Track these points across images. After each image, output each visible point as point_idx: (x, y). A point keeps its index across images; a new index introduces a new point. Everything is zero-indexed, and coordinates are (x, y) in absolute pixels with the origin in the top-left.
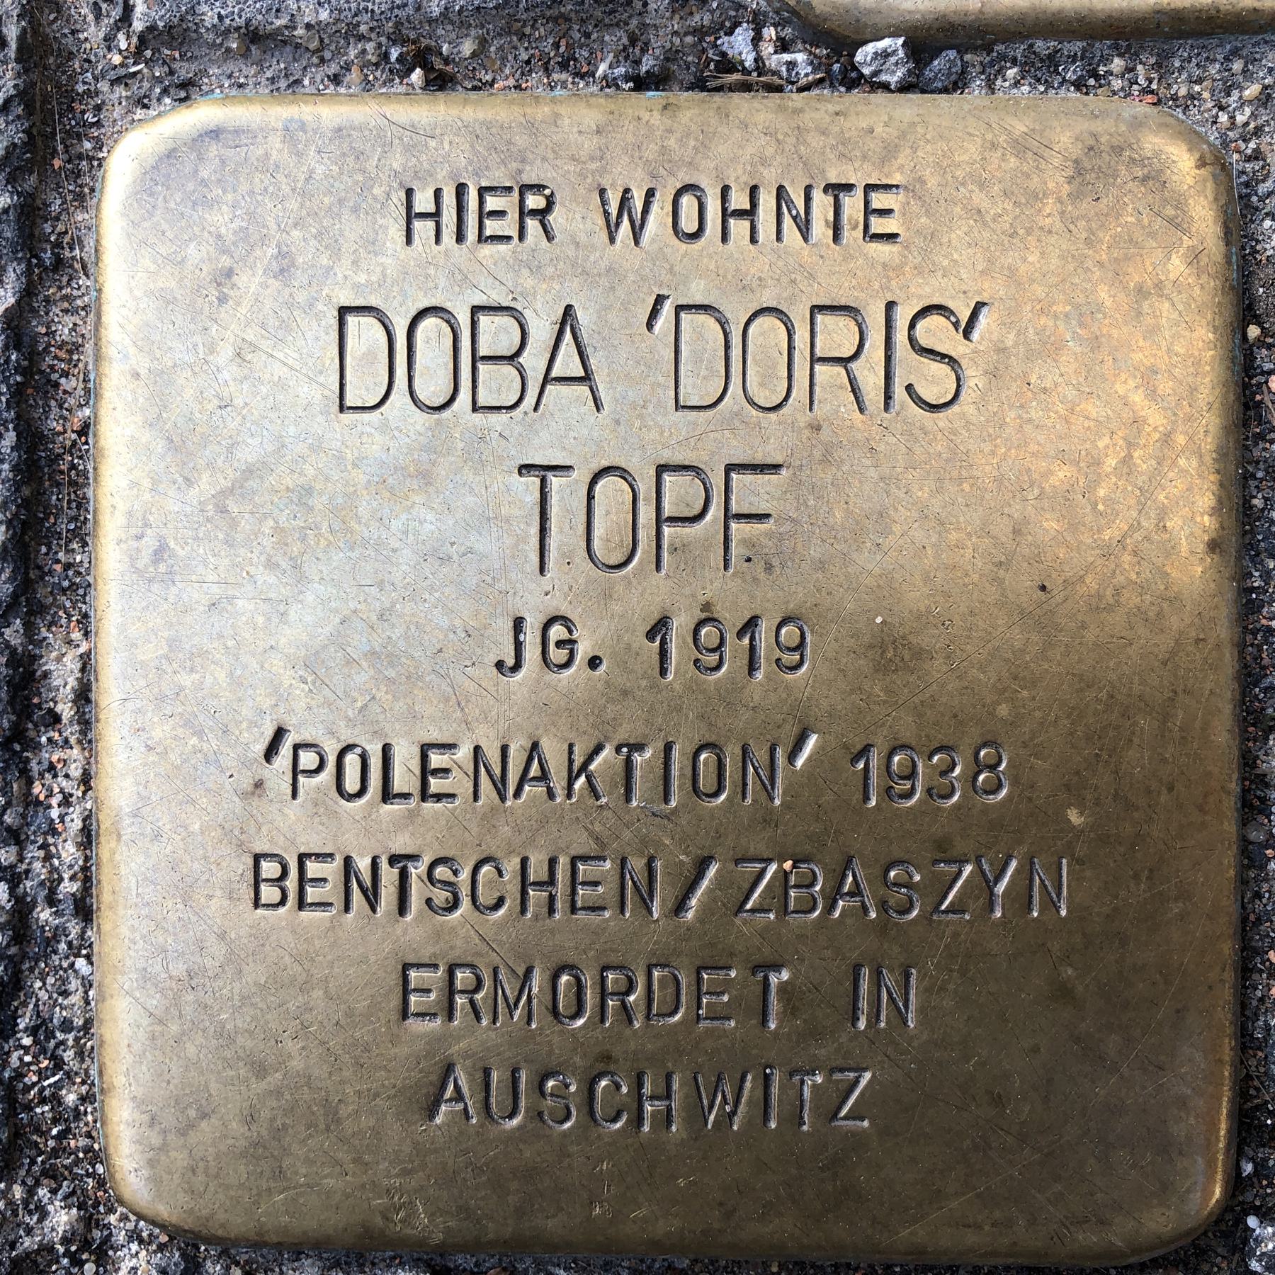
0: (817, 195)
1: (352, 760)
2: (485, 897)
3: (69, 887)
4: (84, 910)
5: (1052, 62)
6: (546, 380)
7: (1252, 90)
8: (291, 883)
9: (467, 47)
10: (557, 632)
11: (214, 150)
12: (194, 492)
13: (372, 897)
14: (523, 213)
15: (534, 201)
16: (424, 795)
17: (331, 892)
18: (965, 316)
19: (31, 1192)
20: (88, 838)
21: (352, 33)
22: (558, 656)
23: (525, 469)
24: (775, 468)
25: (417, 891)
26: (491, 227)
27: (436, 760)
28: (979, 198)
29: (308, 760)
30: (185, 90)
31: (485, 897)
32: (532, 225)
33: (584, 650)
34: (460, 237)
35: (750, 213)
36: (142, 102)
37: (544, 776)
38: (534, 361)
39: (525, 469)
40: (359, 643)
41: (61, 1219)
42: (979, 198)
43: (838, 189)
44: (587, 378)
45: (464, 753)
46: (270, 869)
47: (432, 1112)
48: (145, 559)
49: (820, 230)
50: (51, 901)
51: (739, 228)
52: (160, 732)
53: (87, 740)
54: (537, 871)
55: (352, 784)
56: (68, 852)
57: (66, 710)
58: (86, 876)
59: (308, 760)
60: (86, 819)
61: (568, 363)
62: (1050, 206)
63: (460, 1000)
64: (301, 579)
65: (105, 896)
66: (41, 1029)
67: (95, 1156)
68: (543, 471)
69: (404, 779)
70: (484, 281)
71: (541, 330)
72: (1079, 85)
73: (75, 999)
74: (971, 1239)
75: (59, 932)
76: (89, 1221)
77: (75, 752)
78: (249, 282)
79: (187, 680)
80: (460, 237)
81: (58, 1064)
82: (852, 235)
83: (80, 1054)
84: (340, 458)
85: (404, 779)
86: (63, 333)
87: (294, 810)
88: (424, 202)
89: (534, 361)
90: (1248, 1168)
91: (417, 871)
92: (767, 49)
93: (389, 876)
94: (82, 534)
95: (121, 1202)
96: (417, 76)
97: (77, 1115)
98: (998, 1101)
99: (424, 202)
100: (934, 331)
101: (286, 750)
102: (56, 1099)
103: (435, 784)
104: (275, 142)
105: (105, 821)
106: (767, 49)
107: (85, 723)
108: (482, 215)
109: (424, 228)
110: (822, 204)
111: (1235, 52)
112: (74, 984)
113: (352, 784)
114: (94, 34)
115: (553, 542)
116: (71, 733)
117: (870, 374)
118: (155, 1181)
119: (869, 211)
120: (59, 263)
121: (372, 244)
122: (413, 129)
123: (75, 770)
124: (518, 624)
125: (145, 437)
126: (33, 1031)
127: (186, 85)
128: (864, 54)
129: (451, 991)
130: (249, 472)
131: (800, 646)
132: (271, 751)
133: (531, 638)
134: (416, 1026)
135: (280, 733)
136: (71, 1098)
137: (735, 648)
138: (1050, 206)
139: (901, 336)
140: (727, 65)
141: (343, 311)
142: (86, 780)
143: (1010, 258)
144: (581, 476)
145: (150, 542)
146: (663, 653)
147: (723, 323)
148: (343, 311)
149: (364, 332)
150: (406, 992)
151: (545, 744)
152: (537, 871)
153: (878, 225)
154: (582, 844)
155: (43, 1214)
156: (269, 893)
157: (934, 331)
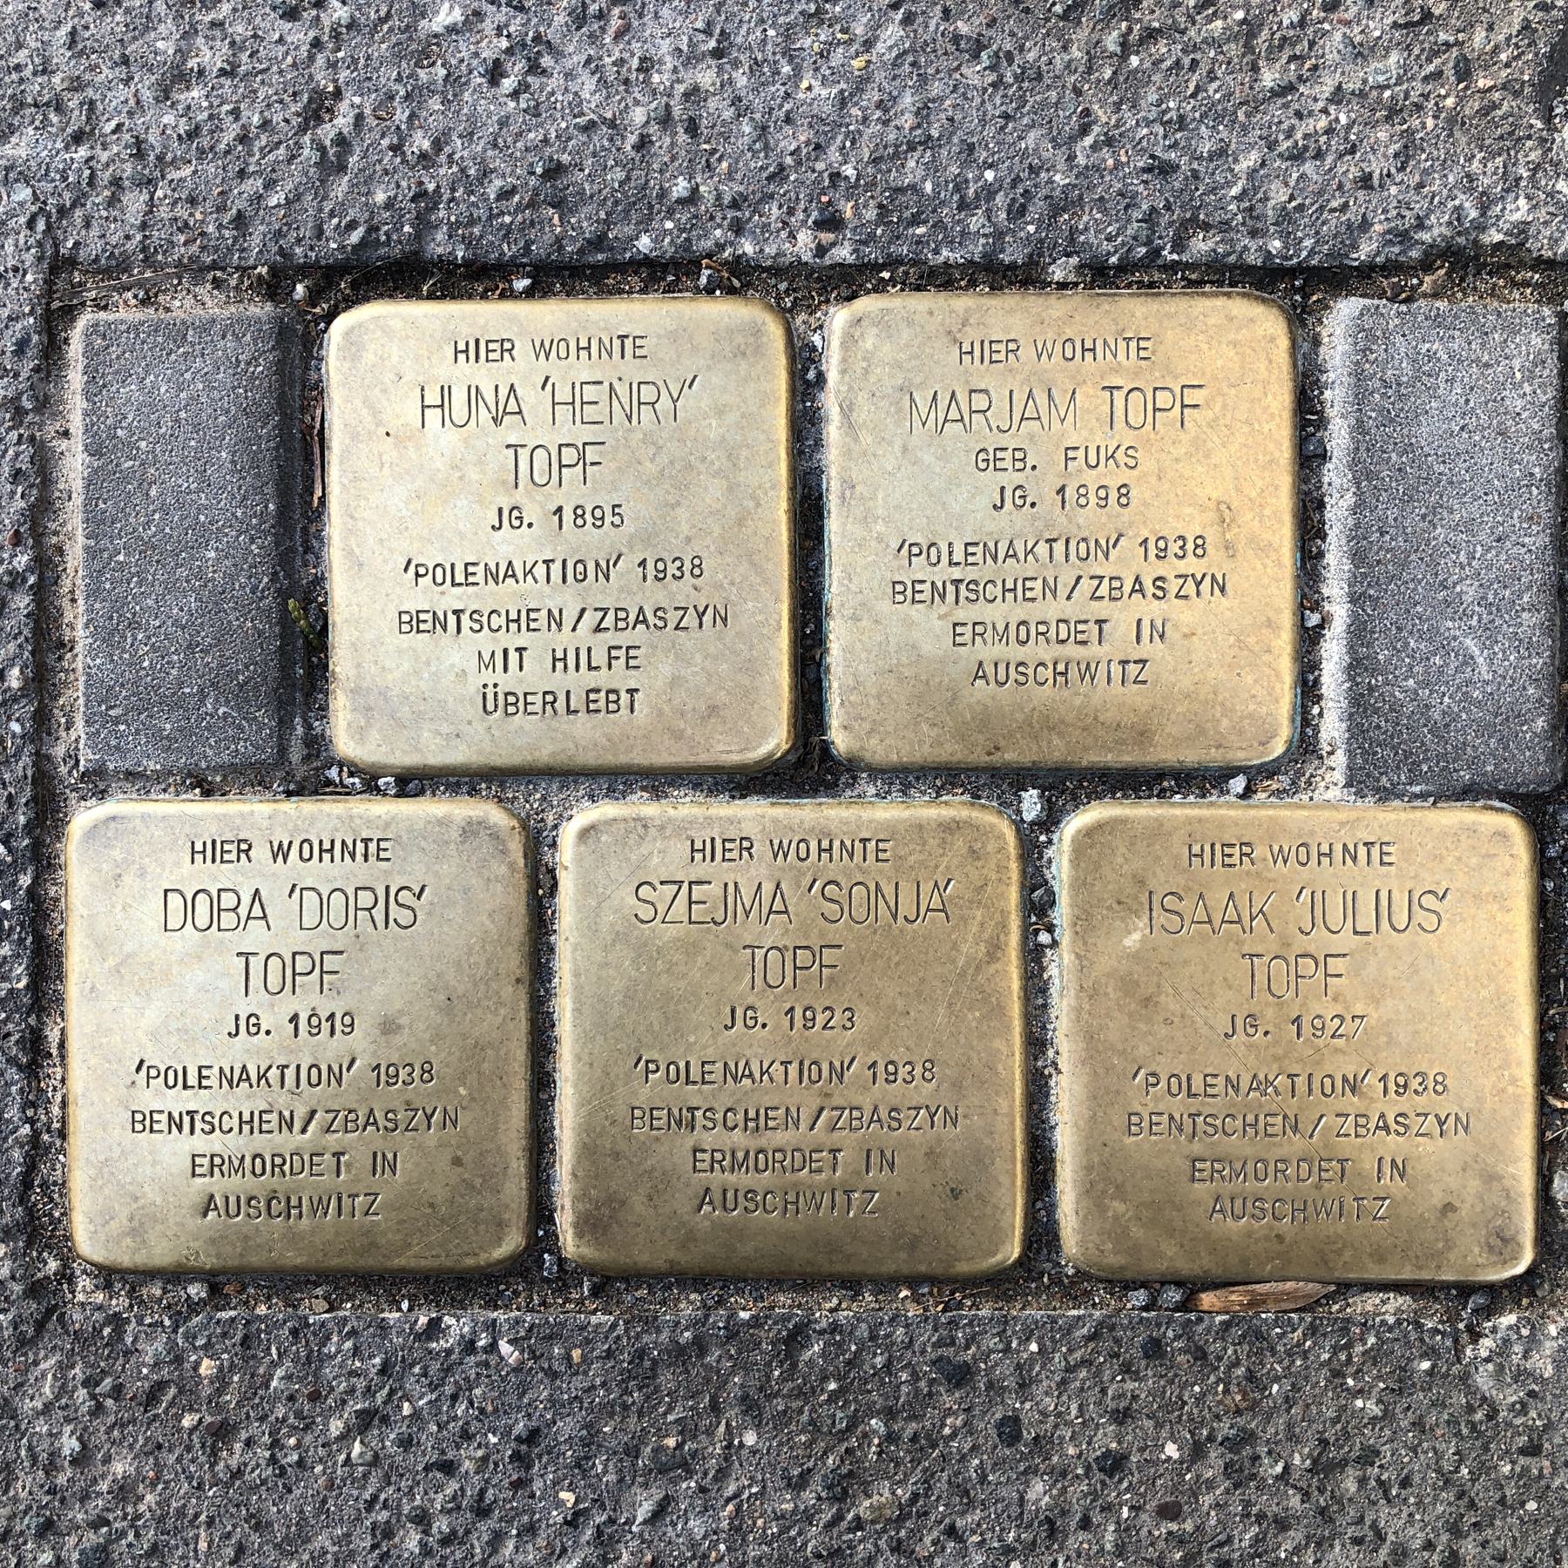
0: (358, 843)
1: (171, 1074)
2: (225, 1128)
3: (56, 1125)
4: (63, 1134)
5: (458, 784)
6: (248, 918)
7: (538, 796)
8: (147, 1122)
9: (218, 779)
10: (253, 1020)
11: (112, 825)
12: (106, 965)
13: (180, 1128)
14: (239, 851)
15: (244, 846)
16: (200, 1087)
17: (164, 1126)
18: (417, 892)
19: (40, 1253)
20: (64, 1104)
21: (170, 773)
22: (253, 1030)
23: (239, 954)
24: (341, 953)
25: (383, 1078)
26: (226, 857)
27: (205, 1072)
28: (423, 844)
29: (153, 1073)
30: (102, 795)
31: (225, 1128)
32: (243, 856)
33: (264, 1028)
34: (214, 861)
35: (331, 850)
36: (84, 798)
37: (248, 1078)
38: (243, 911)
39: (239, 954)
40: (174, 1025)
41: (53, 1265)
42: (423, 844)
43: (366, 841)
44: (265, 917)
45: (216, 1070)
46: (139, 1117)
47: (205, 1215)
48: (87, 991)
49: (359, 857)
50: (49, 1131)
51: (327, 856)
52: (92, 1062)
53: (64, 1065)
54: (246, 1117)
55: (171, 1083)
56: (56, 1111)
57: (54, 1052)
58: (64, 1120)
59: (153, 1073)
60: (64, 1097)
61: (257, 911)
62: (452, 846)
63: (216, 1170)
64: (149, 999)
65: (71, 1128)
66: (44, 1185)
67: (68, 1238)
68: (246, 955)
69: (192, 1080)
70: (223, 879)
71: (246, 899)
72: (469, 794)
73: (59, 1172)
74: (423, 1263)
75: (52, 1144)
76: (65, 1266)
77: (59, 1069)
78: (127, 879)
79: (104, 1040)
80: (214, 861)
81: (51, 1200)
82: (372, 859)
83: (61, 1196)
84: (165, 951)
85: (192, 1080)
86: (52, 893)
87: (148, 1093)
88: (199, 847)
89: (243, 911)
90: (541, 1233)
91: (198, 1117)
92: (345, 775)
93: (186, 1119)
94: (61, 977)
95: (79, 1256)
96: (197, 791)
97: (60, 1221)
98: (432, 1205)
99: (199, 847)
100: (405, 897)
101: (144, 1069)
102: (51, 1215)
103: (205, 1083)
104: (138, 821)
105: (71, 1098)
106: (345, 775)
107: (63, 1057)
108: (222, 852)
109: (462, 357)
110: (360, 847)
111: (529, 782)
112: (58, 1166)
113: (171, 1083)
114: (63, 770)
115: (251, 984)
116: (57, 1061)
117: (379, 913)
118: (93, 1246)
119: (379, 849)
120: (49, 864)
121: (177, 864)
122: (194, 817)
123: (59, 1077)
124: (237, 1018)
125: (86, 942)
126: (40, 1186)
127: (103, 792)
128: (381, 782)
129: (212, 1165)
130: (129, 956)
131: (352, 1024)
132: (138, 1069)
133: (1008, 493)
134: (198, 1180)
135: (142, 1062)
136: (57, 1214)
137: (326, 1026)
138: (452, 846)
139: (392, 899)
140: (329, 782)
141: (166, 891)
142: (63, 1081)
143: (437, 867)
144: (262, 957)
145: (88, 985)
146: (296, 1029)
147: (320, 895)
148: (166, 891)
149: (175, 901)
150: (194, 1165)
151: (249, 1067)
152: (246, 1117)
153: (382, 854)
154: (264, 1106)
155: (46, 1263)
156: (139, 1127)
157: (405, 897)
